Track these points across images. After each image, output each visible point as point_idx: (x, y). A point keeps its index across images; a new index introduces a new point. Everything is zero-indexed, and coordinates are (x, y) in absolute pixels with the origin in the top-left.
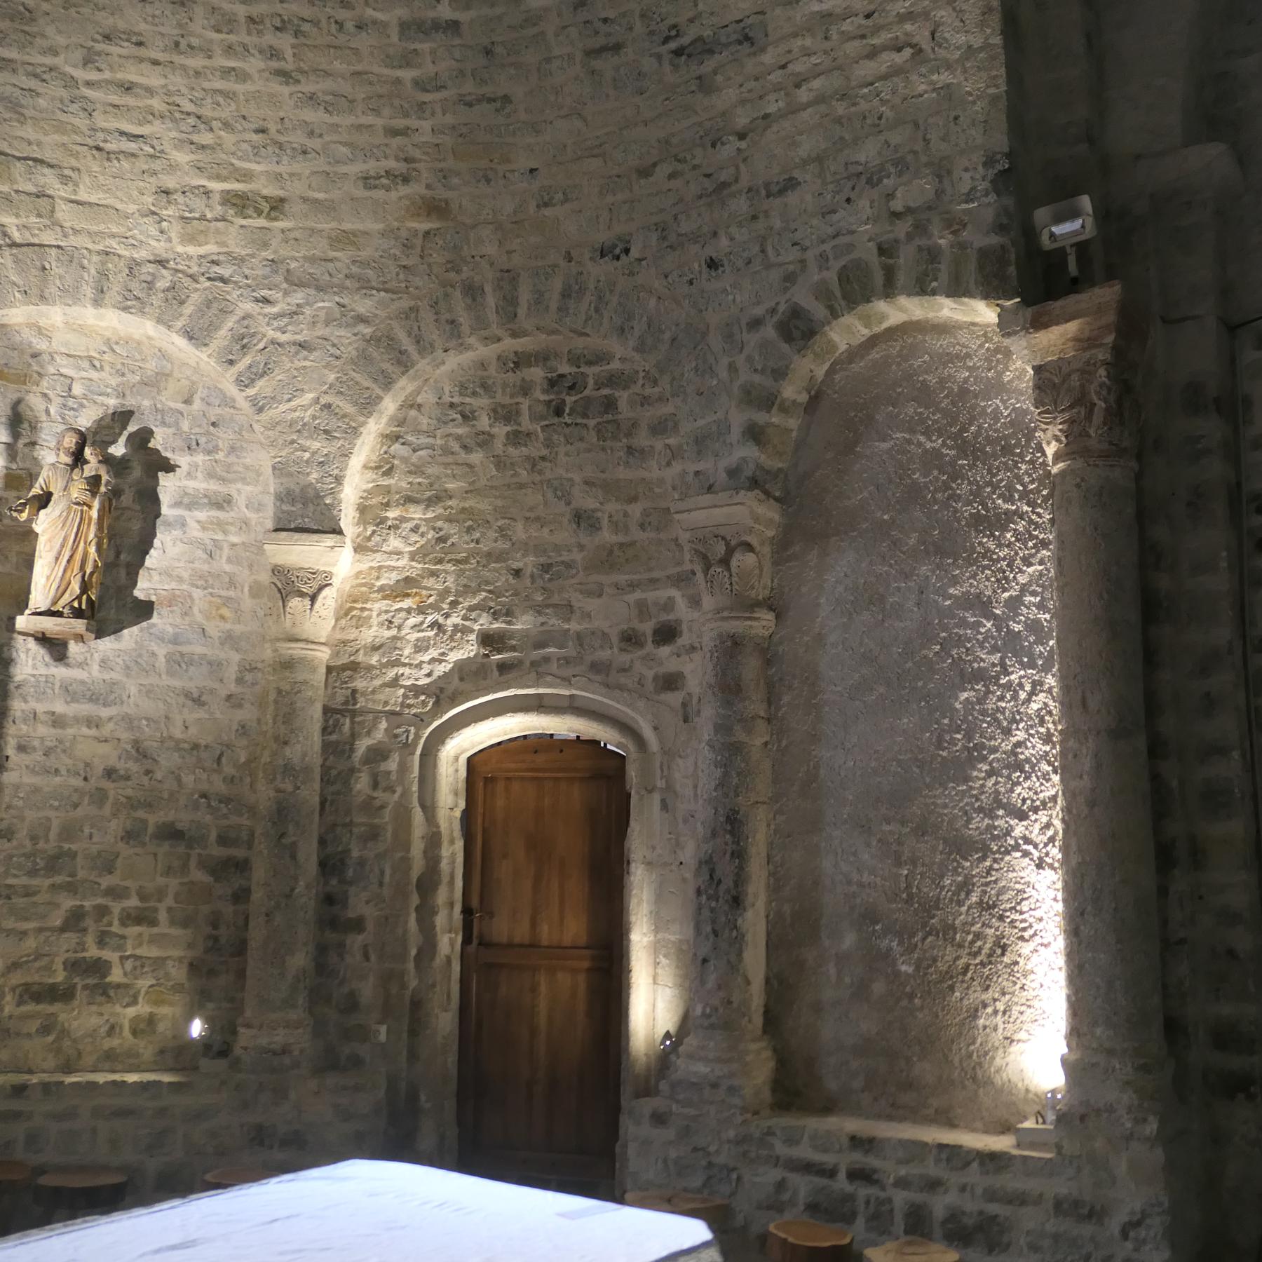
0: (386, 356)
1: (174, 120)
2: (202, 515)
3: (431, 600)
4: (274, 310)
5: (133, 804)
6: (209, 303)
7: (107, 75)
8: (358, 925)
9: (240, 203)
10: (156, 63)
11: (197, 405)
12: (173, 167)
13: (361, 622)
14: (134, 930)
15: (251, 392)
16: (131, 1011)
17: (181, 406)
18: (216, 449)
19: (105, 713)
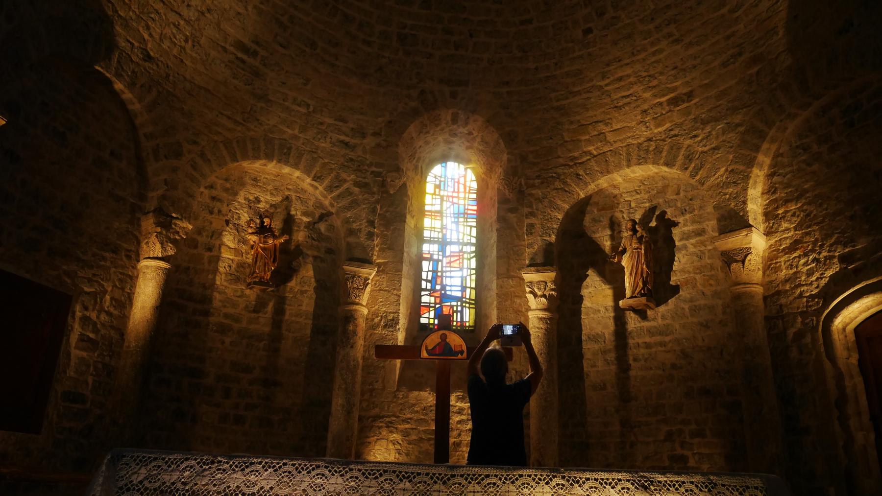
1: (640, 82)
2: (693, 241)
3: (810, 247)
4: (700, 138)
6: (672, 148)
7: (612, 78)
9: (674, 102)
10: (627, 64)
11: (682, 194)
12: (645, 101)
13: (777, 269)
15: (698, 178)
17: (675, 197)
18: (694, 210)
19: (667, 339)
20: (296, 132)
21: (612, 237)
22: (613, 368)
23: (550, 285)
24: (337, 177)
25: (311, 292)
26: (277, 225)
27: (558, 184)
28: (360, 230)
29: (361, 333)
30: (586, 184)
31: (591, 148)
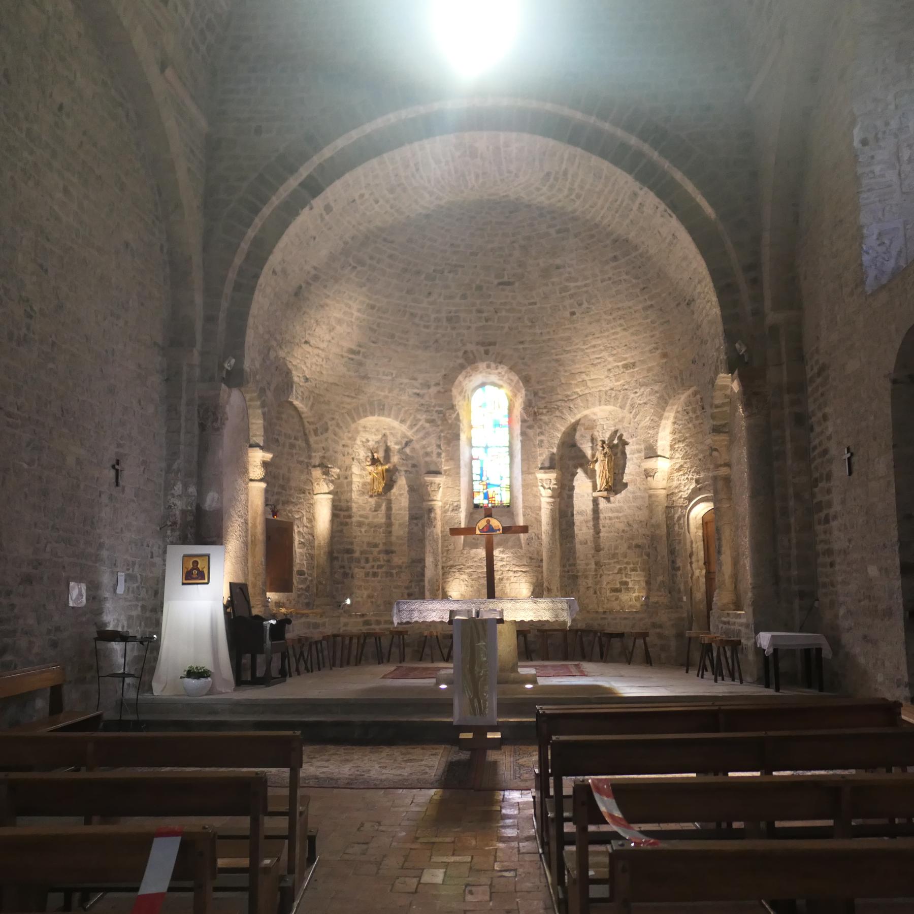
0: (663, 403)
5: (629, 539)
8: (679, 569)
9: (626, 367)
12: (609, 363)
14: (633, 573)
16: (634, 595)
20: (386, 393)
21: (592, 448)
22: (592, 531)
23: (554, 482)
24: (415, 417)
25: (406, 494)
26: (380, 455)
27: (558, 413)
28: (432, 452)
29: (439, 517)
30: (575, 414)
31: (578, 390)
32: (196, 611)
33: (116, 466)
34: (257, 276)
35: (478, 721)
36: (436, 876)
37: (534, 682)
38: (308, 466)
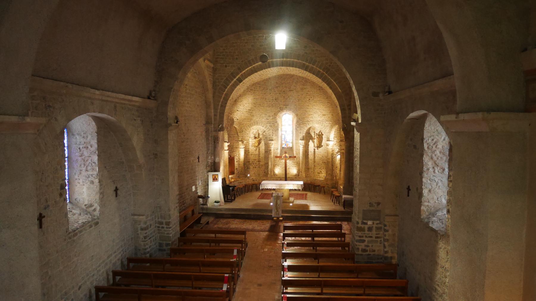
0: (332, 127)
26: (257, 136)
32: (215, 189)
33: (198, 158)
34: (226, 103)
35: (277, 216)
36: (266, 250)
37: (293, 202)
38: (238, 141)
